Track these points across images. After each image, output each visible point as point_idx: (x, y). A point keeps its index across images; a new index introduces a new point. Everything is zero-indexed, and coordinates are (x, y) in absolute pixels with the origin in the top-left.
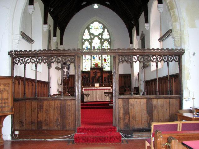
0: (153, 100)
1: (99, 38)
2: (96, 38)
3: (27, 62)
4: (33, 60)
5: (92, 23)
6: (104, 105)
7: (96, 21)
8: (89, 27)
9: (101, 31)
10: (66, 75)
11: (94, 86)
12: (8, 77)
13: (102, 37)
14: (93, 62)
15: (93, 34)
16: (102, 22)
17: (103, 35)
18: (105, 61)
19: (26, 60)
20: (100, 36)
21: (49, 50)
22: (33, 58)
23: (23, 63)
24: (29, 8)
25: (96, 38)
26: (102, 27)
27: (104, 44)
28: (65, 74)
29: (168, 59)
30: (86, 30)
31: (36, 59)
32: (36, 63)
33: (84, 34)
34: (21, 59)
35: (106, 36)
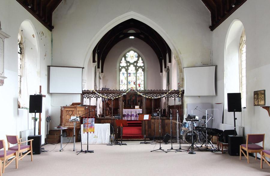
0: (165, 120)
1: (134, 66)
2: (132, 66)
5: (129, 52)
6: (136, 125)
7: (132, 50)
9: (136, 59)
11: (134, 108)
12: (43, 97)
14: (128, 86)
15: (129, 62)
17: (138, 63)
18: (139, 86)
20: (135, 64)
25: (132, 66)
26: (137, 56)
27: (138, 70)
29: (175, 96)
30: (123, 59)
32: (97, 97)
33: (121, 62)
34: (88, 95)
35: (140, 63)
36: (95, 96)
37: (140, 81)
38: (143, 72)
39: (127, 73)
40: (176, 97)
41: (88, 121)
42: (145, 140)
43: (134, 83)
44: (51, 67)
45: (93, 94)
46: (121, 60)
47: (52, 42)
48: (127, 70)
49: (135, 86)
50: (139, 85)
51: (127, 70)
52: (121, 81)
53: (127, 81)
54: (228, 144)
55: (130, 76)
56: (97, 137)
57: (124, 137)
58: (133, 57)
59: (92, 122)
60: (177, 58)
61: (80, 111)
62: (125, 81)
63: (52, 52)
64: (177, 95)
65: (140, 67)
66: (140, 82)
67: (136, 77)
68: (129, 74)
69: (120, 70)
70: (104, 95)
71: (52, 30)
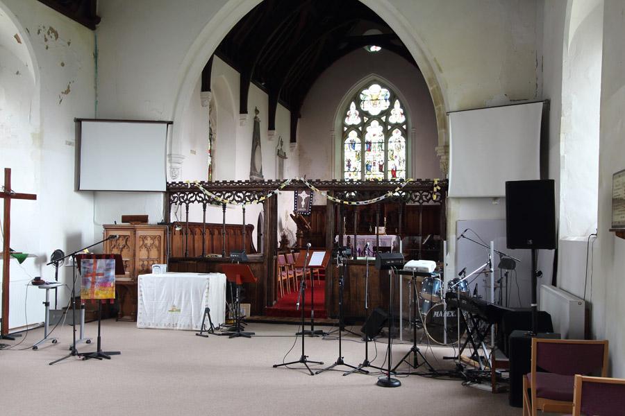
1: (381, 123)
2: (375, 123)
3: (191, 200)
5: (367, 87)
7: (375, 82)
8: (359, 96)
9: (385, 105)
10: (306, 206)
13: (387, 119)
15: (367, 114)
16: (387, 84)
19: (189, 197)
20: (384, 118)
23: (185, 202)
25: (375, 123)
26: (388, 97)
27: (391, 135)
28: (303, 203)
29: (421, 198)
30: (353, 105)
35: (397, 116)
36: (201, 199)
37: (396, 162)
38: (403, 140)
39: (363, 143)
40: (424, 201)
41: (95, 268)
42: (313, 324)
43: (381, 167)
44: (82, 122)
45: (232, 194)
46: (348, 109)
47: (96, 56)
48: (361, 135)
49: (383, 176)
50: (394, 172)
51: (361, 135)
52: (346, 163)
53: (363, 162)
55: (370, 150)
56: (179, 310)
57: (275, 313)
58: (377, 99)
59: (108, 270)
60: (432, 86)
61: (149, 239)
62: (356, 164)
63: (96, 84)
65: (397, 126)
66: (397, 164)
67: (386, 151)
68: (365, 145)
69: (345, 135)
70: (224, 195)
71: (97, 26)
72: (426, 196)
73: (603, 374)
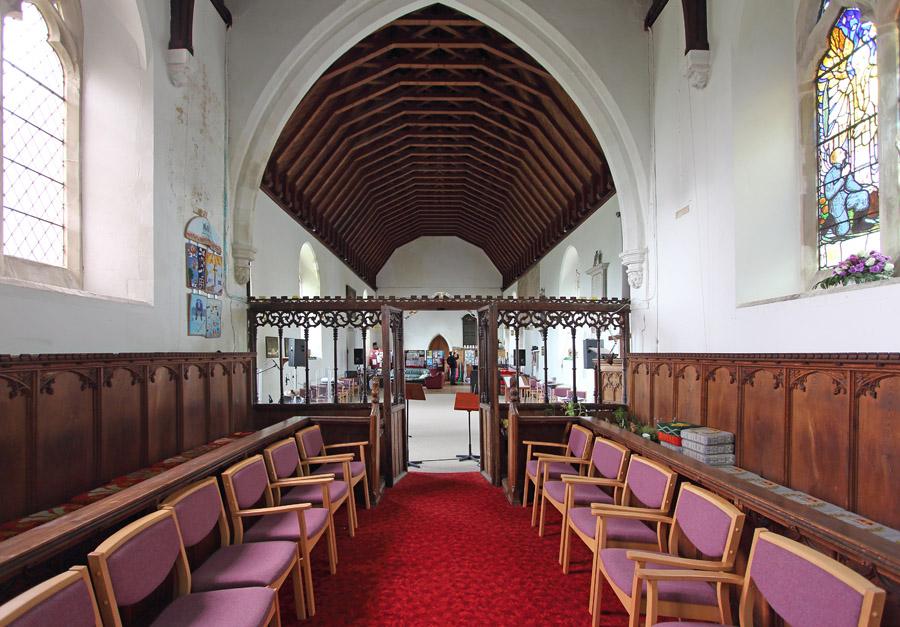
4: (592, 319)
21: (604, 299)
22: (591, 315)
23: (569, 325)
24: (51, 251)
29: (281, 320)
31: (598, 316)
32: (598, 326)
36: (593, 322)
54: (540, 534)
64: (313, 319)
72: (287, 318)
73: (740, 583)
